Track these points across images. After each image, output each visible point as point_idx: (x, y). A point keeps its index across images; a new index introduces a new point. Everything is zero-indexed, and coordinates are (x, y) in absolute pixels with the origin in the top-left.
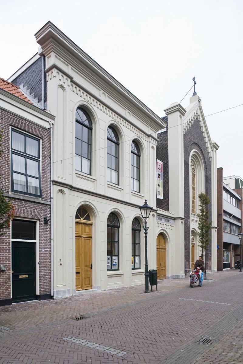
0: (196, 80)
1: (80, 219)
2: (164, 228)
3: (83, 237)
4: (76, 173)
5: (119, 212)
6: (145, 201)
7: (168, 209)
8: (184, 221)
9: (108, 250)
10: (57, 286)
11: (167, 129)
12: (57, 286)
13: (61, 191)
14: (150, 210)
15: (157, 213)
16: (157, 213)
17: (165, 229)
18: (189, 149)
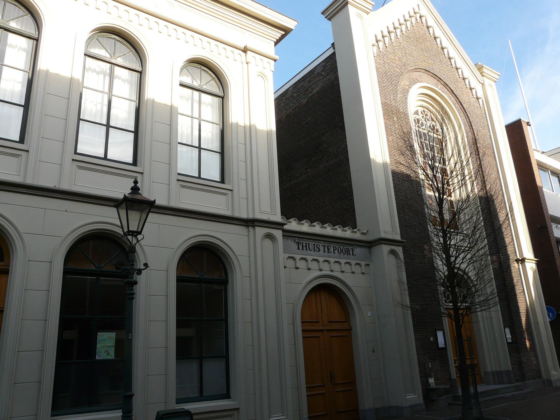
2: (332, 271)
4: (178, 180)
6: (133, 185)
8: (401, 248)
9: (177, 337)
13: (269, 236)
15: (284, 231)
16: (284, 231)
17: (337, 274)
18: (404, 82)
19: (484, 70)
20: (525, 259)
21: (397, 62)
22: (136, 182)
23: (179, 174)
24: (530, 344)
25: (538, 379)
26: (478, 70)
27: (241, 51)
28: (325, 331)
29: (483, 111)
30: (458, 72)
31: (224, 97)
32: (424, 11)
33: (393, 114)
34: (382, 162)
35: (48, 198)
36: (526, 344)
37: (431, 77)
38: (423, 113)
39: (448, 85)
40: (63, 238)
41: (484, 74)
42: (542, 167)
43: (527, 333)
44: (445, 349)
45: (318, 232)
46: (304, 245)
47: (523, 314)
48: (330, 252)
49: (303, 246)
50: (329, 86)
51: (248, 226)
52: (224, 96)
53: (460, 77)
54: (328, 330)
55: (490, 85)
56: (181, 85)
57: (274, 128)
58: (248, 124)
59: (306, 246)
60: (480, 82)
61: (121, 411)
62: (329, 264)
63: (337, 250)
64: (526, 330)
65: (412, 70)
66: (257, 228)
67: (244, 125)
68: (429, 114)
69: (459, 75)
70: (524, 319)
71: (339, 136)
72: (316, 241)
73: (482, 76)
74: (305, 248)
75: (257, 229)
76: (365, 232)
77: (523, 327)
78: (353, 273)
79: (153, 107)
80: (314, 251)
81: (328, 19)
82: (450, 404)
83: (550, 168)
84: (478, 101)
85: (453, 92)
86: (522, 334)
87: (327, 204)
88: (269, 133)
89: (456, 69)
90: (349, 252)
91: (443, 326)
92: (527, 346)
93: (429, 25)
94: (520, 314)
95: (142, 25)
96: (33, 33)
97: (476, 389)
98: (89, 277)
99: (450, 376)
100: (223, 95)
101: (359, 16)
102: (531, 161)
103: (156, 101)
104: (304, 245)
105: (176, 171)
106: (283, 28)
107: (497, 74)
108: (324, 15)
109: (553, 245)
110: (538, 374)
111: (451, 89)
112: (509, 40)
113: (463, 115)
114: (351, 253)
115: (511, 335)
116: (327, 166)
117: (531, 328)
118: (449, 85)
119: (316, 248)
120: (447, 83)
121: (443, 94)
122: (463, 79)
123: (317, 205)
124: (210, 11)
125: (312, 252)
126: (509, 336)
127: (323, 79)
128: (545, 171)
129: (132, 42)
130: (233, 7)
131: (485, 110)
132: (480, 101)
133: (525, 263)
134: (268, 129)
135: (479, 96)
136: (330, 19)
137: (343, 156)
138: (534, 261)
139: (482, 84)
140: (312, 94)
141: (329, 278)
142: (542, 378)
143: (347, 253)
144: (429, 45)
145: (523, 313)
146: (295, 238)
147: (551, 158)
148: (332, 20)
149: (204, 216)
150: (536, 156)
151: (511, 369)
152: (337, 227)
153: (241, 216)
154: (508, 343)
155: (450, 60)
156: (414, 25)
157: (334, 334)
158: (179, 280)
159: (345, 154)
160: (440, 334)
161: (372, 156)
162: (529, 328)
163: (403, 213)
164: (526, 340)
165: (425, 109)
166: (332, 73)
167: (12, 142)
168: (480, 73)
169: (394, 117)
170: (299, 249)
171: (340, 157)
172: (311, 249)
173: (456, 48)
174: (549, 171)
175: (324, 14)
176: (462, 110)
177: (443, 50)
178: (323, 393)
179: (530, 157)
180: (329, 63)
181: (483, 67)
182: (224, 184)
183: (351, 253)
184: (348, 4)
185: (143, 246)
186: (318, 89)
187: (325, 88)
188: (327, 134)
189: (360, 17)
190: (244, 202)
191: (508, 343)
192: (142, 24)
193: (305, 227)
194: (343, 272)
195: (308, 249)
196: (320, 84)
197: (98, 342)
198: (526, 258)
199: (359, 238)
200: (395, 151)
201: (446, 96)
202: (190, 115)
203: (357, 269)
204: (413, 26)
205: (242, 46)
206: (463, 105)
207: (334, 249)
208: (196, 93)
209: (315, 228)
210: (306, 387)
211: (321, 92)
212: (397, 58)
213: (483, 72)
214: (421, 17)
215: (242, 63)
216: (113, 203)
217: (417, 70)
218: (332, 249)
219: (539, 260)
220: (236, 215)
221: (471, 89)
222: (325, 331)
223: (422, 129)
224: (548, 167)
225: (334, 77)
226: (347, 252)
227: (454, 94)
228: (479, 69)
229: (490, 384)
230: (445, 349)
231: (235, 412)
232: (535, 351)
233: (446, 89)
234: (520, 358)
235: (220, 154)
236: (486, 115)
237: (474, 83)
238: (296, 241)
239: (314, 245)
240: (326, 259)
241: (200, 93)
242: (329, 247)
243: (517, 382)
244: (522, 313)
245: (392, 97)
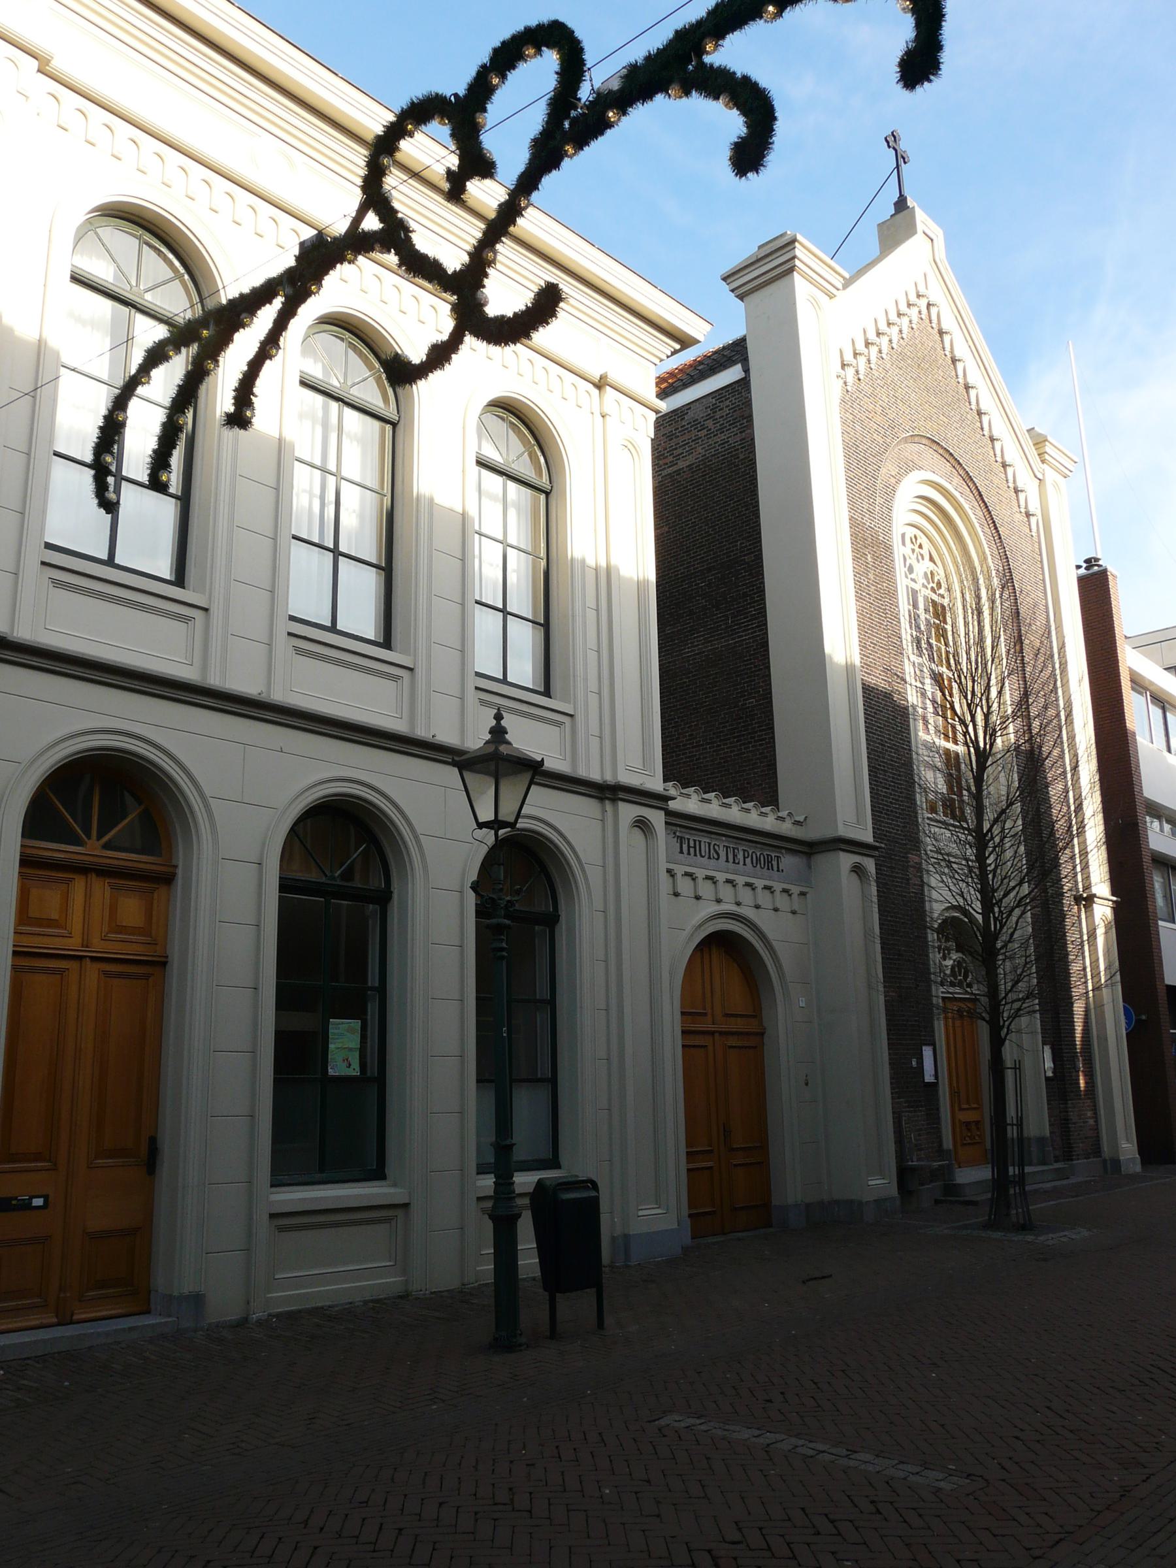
0: (903, 146)
1: (77, 842)
2: (738, 904)
3: (94, 959)
4: (290, 634)
5: (551, 842)
6: (494, 722)
7: (769, 797)
10: (641, 1213)
11: (747, 370)
12: (641, 1213)
14: (527, 777)
15: (669, 813)
16: (669, 813)
18: (888, 468)
19: (1048, 448)
20: (1095, 896)
21: (879, 419)
22: (498, 717)
23: (49, 546)
24: (1086, 1083)
25: (1094, 1157)
26: (1034, 445)
27: (591, 385)
28: (717, 1035)
29: (1036, 545)
30: (993, 448)
31: (397, 424)
32: (936, 293)
33: (865, 547)
34: (845, 663)
35: (81, 682)
36: (1079, 1083)
37: (940, 457)
38: (914, 540)
39: (972, 479)
40: (23, 765)
41: (1047, 457)
42: (1139, 684)
43: (1083, 1060)
44: (934, 1085)
45: (738, 821)
46: (692, 844)
47: (1078, 1018)
48: (737, 861)
49: (689, 847)
50: (723, 460)
51: (601, 799)
52: (551, 490)
53: (996, 461)
54: (721, 1033)
55: (1056, 485)
56: (78, 279)
57: (652, 576)
58: (603, 563)
59: (695, 847)
60: (1036, 477)
61: (493, 1176)
62: (771, 895)
63: (750, 858)
64: (1081, 1052)
65: (905, 440)
66: (621, 805)
67: (594, 566)
68: (927, 545)
69: (995, 455)
70: (1080, 1028)
71: (743, 585)
72: (713, 836)
73: (1041, 461)
74: (692, 850)
75: (622, 806)
76: (801, 819)
77: (1076, 1045)
78: (776, 910)
79: (431, 515)
80: (709, 858)
81: (737, 297)
83: (1151, 688)
84: (1029, 521)
85: (981, 495)
86: (1074, 1061)
87: (700, 741)
88: (641, 585)
89: (991, 441)
90: (772, 865)
91: (934, 1036)
92: (1080, 1087)
93: (945, 327)
94: (1073, 1018)
95: (193, 200)
96: (126, 289)
97: (1023, 1170)
98: (346, 902)
99: (940, 1145)
100: (397, 418)
101: (813, 301)
102: (1119, 669)
103: (437, 501)
104: (692, 844)
105: (287, 611)
106: (677, 335)
107: (1072, 460)
108: (728, 284)
109: (1145, 867)
110: (1096, 1149)
111: (978, 490)
112: (1070, 342)
113: (997, 553)
114: (775, 868)
115: (1054, 1061)
116: (704, 652)
117: (1090, 1049)
118: (974, 479)
119: (712, 851)
120: (971, 474)
121: (962, 500)
122: (1003, 467)
123: (671, 741)
124: (515, 271)
125: (705, 860)
126: (1049, 1064)
127: (708, 439)
128: (1140, 693)
129: (536, 432)
130: (171, 14)
131: (1039, 543)
132: (1033, 520)
133: (1094, 905)
134: (641, 578)
135: (1032, 510)
136: (741, 297)
137: (749, 634)
138: (1111, 903)
139: (1040, 480)
140: (675, 468)
141: (727, 918)
142: (1101, 1157)
143: (768, 866)
144: (940, 378)
145: (1080, 1015)
146: (674, 828)
147: (1141, 653)
148: (746, 299)
149: (249, 706)
150: (1130, 659)
151: (1048, 1134)
152: (750, 805)
153: (591, 776)
154: (1047, 1079)
155: (980, 418)
156: (914, 326)
157: (733, 1041)
158: (285, 886)
159: (755, 632)
160: (927, 1052)
161: (828, 649)
162: (1087, 1049)
163: (875, 781)
164: (1081, 1074)
165: (919, 533)
166: (735, 429)
167: (143, 576)
168: (1039, 455)
169: (867, 555)
170: (681, 852)
171: (742, 636)
172: (703, 854)
173: (995, 389)
174: (1148, 693)
175: (728, 282)
176: (995, 541)
177: (967, 392)
178: (710, 1168)
179: (1118, 660)
180: (728, 403)
181: (1046, 440)
182: (184, 588)
183: (775, 868)
184: (793, 271)
185: (210, 799)
186: (691, 459)
187: (711, 461)
188: (710, 574)
189: (816, 306)
190: (594, 743)
191: (1047, 1079)
192: (193, 196)
193: (713, 808)
194: (757, 907)
195: (698, 854)
196: (699, 450)
197: (332, 1038)
198: (1098, 895)
199: (789, 833)
200: (865, 636)
201: (966, 506)
202: (501, 537)
203: (781, 901)
204: (912, 329)
205: (596, 376)
206: (999, 529)
207: (744, 855)
208: (334, 405)
209: (711, 806)
210: (687, 1152)
211: (699, 469)
212: (879, 410)
213: (1046, 452)
214: (929, 305)
215: (592, 413)
216: (451, 757)
217: (914, 438)
218: (740, 856)
219: (1119, 899)
220: (212, 682)
221: (1016, 491)
222: (717, 1035)
223: (939, 595)
224: (1147, 684)
225: (738, 439)
227: (984, 502)
228: (1037, 444)
230: (934, 1085)
231: (400, 1213)
232: (1094, 1098)
233: (967, 488)
234: (1067, 1112)
235: (179, 502)
236: (1041, 555)
237: (1025, 481)
238: (678, 834)
239: (709, 844)
240: (731, 877)
241: (341, 408)
242: (736, 851)
243: (1056, 1161)
244: (1077, 1014)
245: (866, 506)
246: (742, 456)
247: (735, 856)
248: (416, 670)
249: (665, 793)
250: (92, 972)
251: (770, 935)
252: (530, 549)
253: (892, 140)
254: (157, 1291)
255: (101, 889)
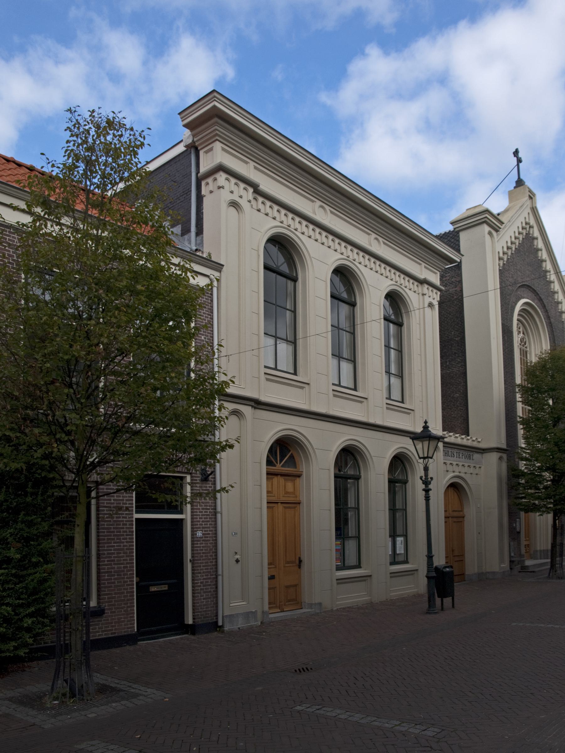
0: (520, 155)
1: (275, 466)
6: (424, 424)
7: (466, 432)
17: (462, 475)
82: (520, 572)
99: (520, 552)
125: (450, 458)
153: (261, 399)
180: (449, 274)
218: (461, 456)
226: (469, 457)
229: (537, 559)
231: (369, 578)
246: (455, 297)
247: (459, 455)
248: (369, 399)
249: (443, 436)
250: (280, 507)
251: (469, 482)
252: (397, 348)
253: (516, 153)
254: (305, 602)
255: (281, 480)
